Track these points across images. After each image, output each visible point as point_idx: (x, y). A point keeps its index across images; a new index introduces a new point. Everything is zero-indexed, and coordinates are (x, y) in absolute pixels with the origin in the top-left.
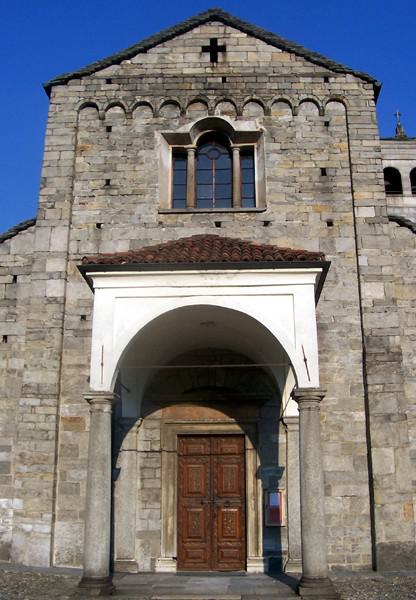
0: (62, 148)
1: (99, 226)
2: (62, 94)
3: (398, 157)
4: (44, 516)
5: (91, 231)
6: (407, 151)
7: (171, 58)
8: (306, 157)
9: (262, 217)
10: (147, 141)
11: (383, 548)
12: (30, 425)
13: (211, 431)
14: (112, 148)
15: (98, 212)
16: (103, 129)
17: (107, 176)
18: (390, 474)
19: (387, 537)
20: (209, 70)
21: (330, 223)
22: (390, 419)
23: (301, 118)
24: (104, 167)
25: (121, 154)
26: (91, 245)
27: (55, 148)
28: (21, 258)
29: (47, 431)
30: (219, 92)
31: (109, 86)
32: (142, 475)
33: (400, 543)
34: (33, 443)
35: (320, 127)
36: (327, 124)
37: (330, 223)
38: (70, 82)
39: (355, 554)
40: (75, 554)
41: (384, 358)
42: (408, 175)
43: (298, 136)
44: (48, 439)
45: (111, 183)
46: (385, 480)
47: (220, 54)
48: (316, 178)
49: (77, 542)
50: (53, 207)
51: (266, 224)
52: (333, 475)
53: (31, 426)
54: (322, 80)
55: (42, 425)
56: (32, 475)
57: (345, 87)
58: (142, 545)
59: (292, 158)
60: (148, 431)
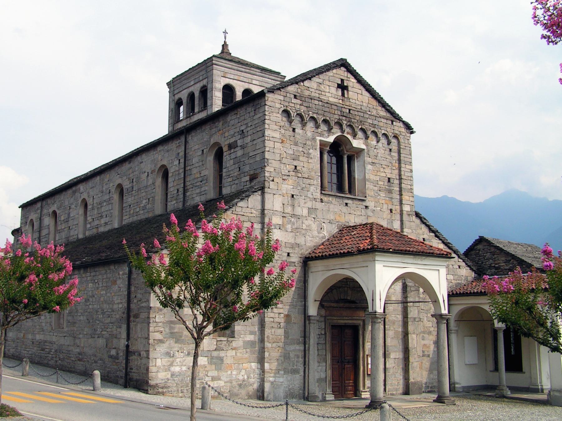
0: (275, 140)
1: (293, 196)
2: (272, 100)
3: (236, 77)
4: (280, 372)
5: (289, 199)
6: (243, 74)
7: (323, 88)
8: (382, 170)
9: (364, 204)
10: (313, 144)
11: (412, 384)
12: (271, 319)
13: (346, 323)
14: (296, 144)
15: (292, 187)
16: (291, 130)
17: (295, 163)
18: (415, 348)
19: (413, 379)
20: (341, 101)
21: (391, 211)
22: (415, 320)
23: (380, 144)
24: (293, 156)
25: (301, 149)
26: (290, 207)
27: (271, 139)
28: (255, 212)
29: (280, 323)
30: (347, 119)
31: (294, 101)
32: (318, 348)
33: (418, 381)
34: (273, 330)
35: (387, 152)
36: (390, 150)
37: (391, 211)
38: (276, 92)
39: (398, 387)
40: (288, 393)
41: (414, 289)
42: (241, 94)
43: (379, 155)
44: (280, 328)
45: (298, 168)
46: (413, 350)
47: (346, 92)
48: (386, 183)
49: (289, 386)
50: (273, 181)
51: (366, 207)
52: (391, 348)
53: (272, 320)
54: (390, 122)
55: (277, 320)
56: (274, 349)
57: (400, 130)
58: (318, 386)
59: (376, 169)
60: (320, 323)
